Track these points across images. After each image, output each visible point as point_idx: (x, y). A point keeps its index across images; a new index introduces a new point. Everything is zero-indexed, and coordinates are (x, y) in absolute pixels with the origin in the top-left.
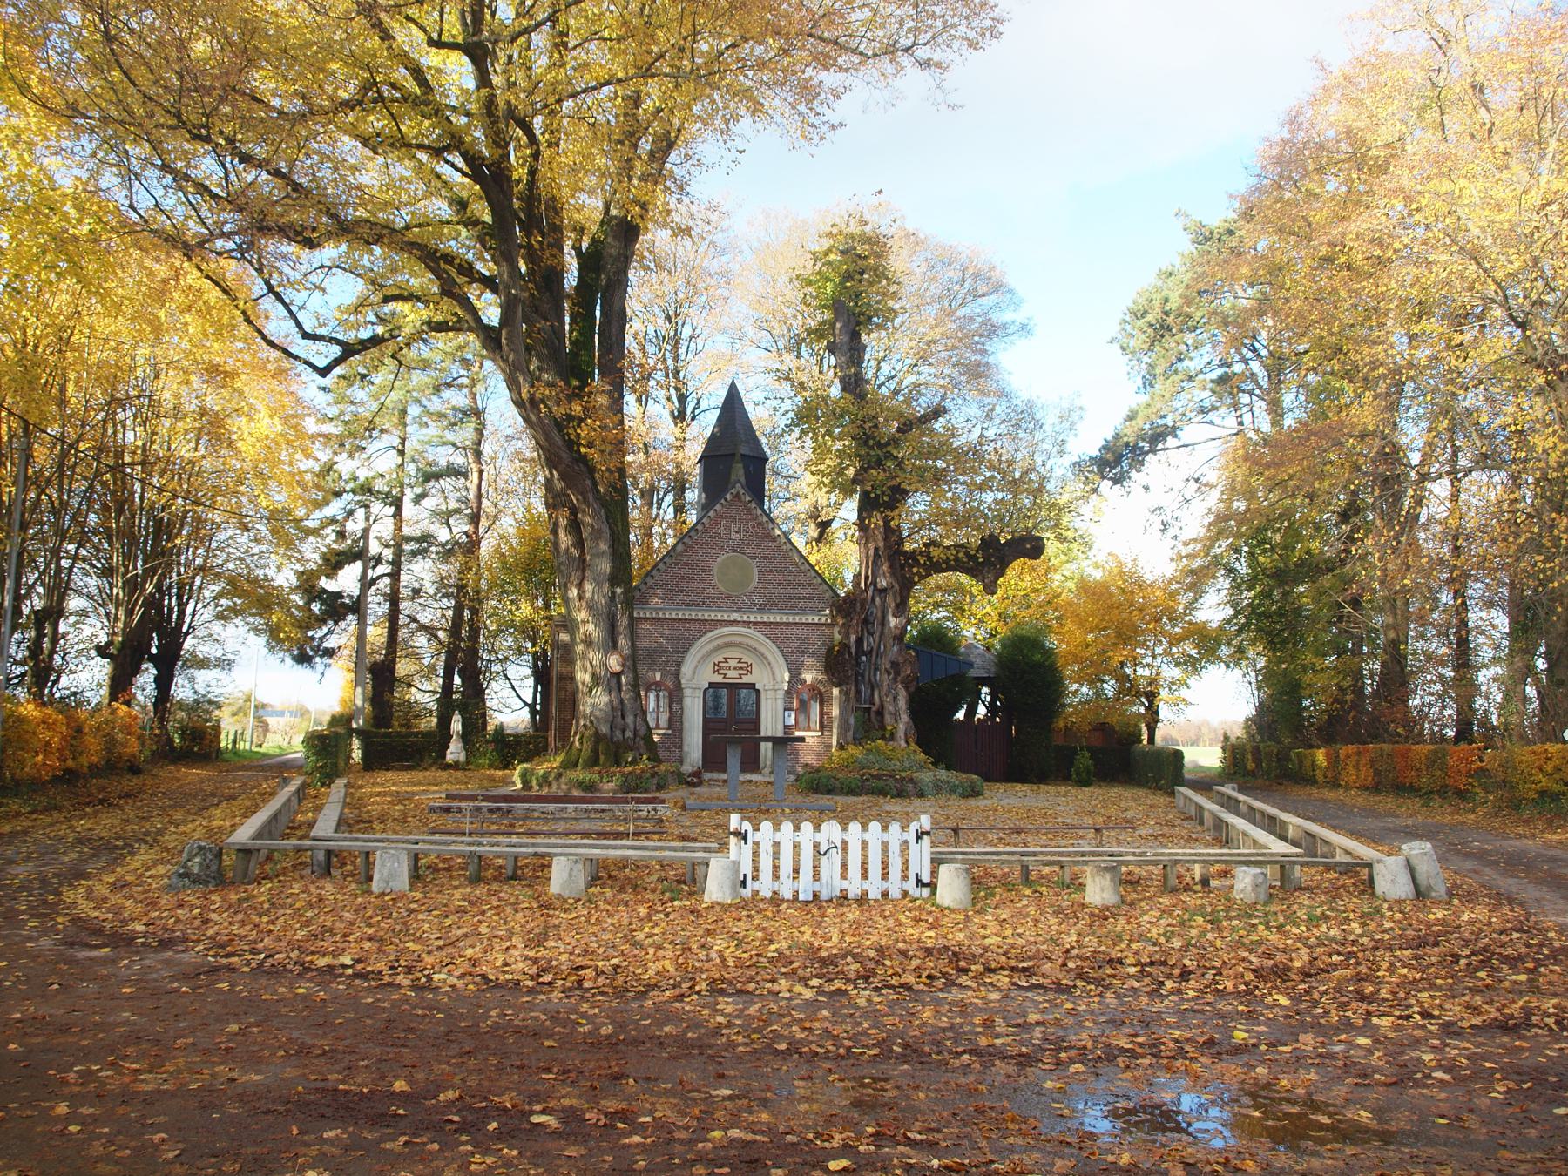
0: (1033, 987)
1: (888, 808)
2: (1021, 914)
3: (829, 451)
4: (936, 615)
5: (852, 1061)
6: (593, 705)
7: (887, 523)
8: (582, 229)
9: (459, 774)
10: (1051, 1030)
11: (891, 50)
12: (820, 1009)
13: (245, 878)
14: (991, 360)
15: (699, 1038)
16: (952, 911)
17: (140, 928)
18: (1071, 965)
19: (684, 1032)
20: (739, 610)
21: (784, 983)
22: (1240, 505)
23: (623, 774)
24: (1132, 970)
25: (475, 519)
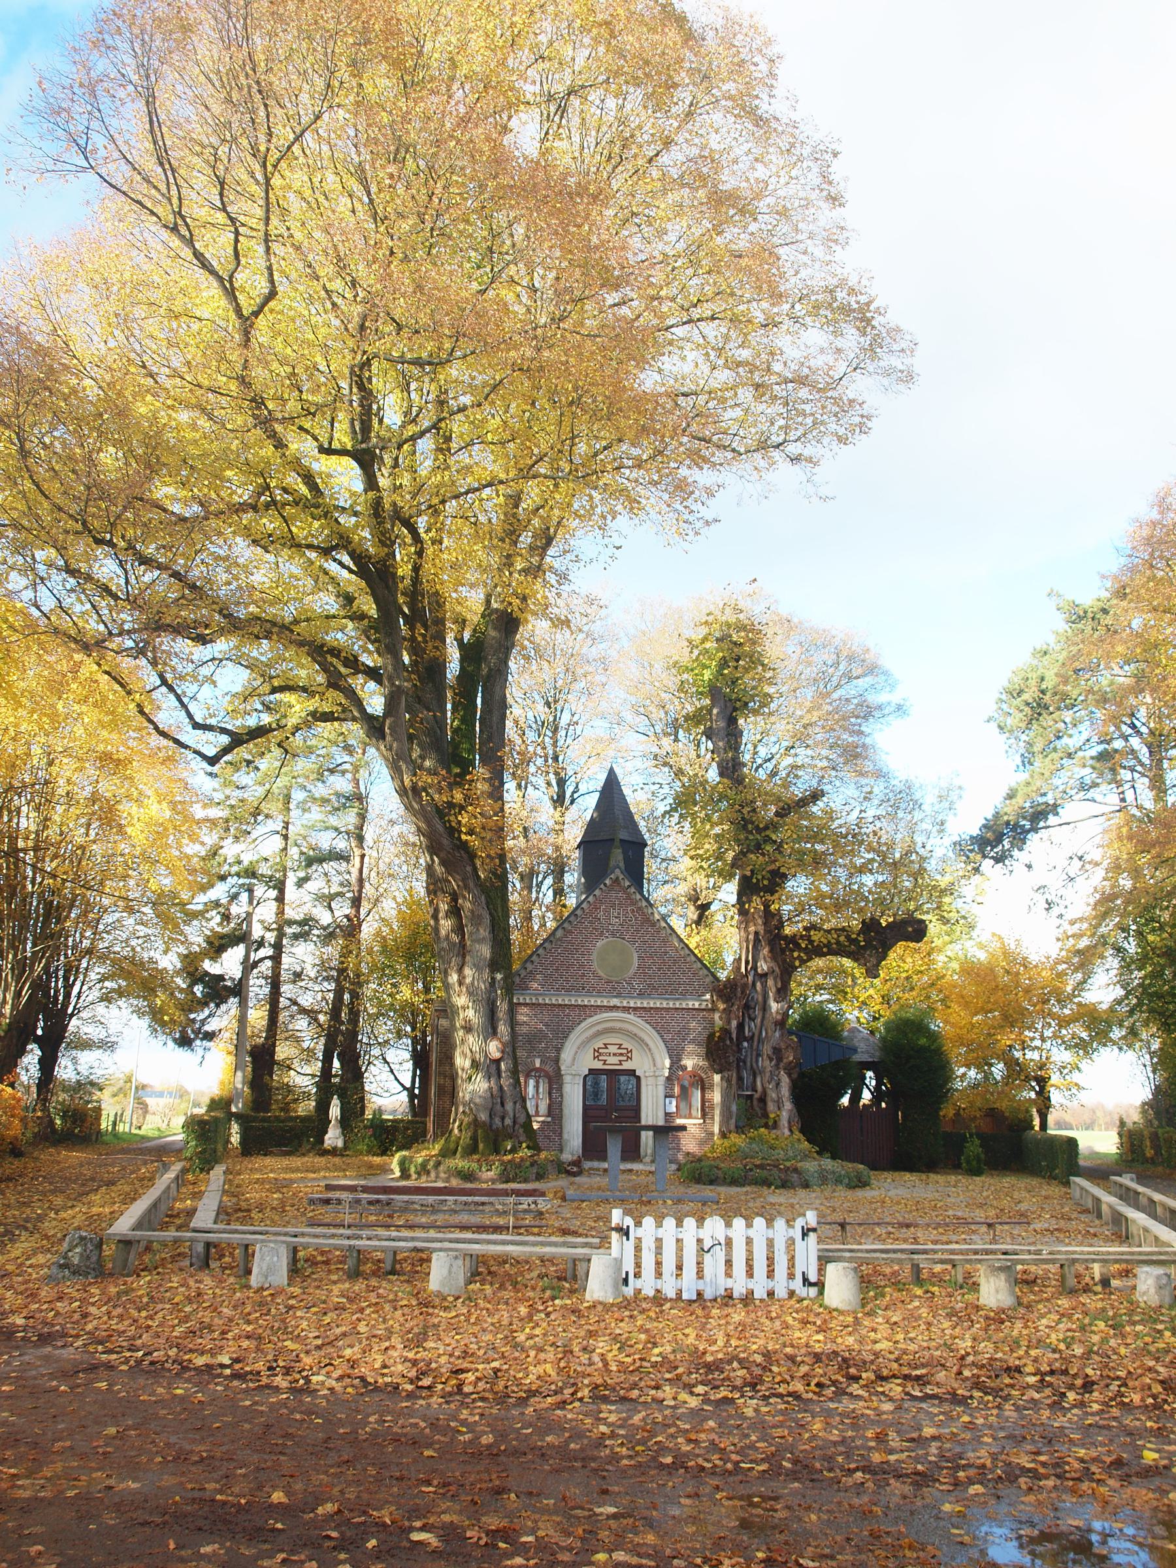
0: (927, 1397)
1: (772, 1199)
2: (913, 1317)
3: (707, 835)
4: (818, 998)
5: (740, 1477)
6: (473, 1092)
7: (767, 906)
8: (464, 621)
9: (337, 1160)
10: (948, 1446)
11: (763, 446)
12: (706, 1419)
13: (124, 1270)
14: (868, 741)
15: (582, 1450)
16: (841, 1312)
17: (20, 1321)
18: (967, 1373)
19: (567, 1442)
20: (618, 996)
21: (668, 1391)
22: (1126, 883)
23: (502, 1163)
24: (1032, 1380)
25: (356, 902)
